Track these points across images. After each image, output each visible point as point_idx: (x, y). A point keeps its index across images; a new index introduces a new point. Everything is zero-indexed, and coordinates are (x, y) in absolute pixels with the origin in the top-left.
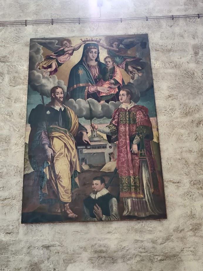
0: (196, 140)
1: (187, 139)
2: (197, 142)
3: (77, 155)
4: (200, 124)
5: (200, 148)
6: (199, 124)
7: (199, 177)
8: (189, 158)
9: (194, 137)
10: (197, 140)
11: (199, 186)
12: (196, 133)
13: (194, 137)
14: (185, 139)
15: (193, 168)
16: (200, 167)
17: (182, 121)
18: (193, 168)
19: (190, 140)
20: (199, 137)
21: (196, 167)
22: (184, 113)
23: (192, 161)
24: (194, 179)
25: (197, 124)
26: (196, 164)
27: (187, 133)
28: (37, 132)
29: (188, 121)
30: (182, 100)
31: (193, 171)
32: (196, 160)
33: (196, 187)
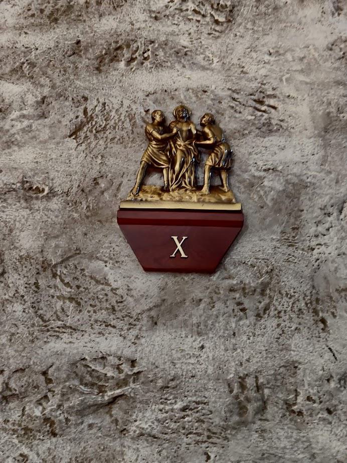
0: (74, 134)
1: (27, 130)
2: (79, 145)
3: (140, 172)
4: (115, 59)
5: (94, 174)
6: (112, 61)
7: (56, 345)
8: (11, 231)
9: (72, 116)
10: (82, 134)
11: (38, 412)
12: (86, 99)
13: (70, 115)
14: (19, 126)
15: (22, 291)
16: (67, 285)
17: (18, 46)
18: (22, 291)
19: (45, 134)
20: (100, 121)
21: (42, 283)
22: (42, 11)
23: (27, 246)
24: (14, 364)
25: (101, 59)
26: (45, 266)
27: (31, 99)
28: (222, 195)
29: (52, 44)
30: (65, 367)
31: (18, 307)
32: (53, 243)
33: (15, 416)
